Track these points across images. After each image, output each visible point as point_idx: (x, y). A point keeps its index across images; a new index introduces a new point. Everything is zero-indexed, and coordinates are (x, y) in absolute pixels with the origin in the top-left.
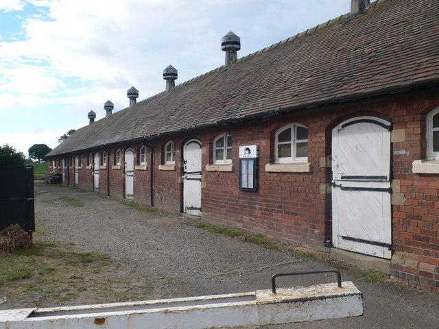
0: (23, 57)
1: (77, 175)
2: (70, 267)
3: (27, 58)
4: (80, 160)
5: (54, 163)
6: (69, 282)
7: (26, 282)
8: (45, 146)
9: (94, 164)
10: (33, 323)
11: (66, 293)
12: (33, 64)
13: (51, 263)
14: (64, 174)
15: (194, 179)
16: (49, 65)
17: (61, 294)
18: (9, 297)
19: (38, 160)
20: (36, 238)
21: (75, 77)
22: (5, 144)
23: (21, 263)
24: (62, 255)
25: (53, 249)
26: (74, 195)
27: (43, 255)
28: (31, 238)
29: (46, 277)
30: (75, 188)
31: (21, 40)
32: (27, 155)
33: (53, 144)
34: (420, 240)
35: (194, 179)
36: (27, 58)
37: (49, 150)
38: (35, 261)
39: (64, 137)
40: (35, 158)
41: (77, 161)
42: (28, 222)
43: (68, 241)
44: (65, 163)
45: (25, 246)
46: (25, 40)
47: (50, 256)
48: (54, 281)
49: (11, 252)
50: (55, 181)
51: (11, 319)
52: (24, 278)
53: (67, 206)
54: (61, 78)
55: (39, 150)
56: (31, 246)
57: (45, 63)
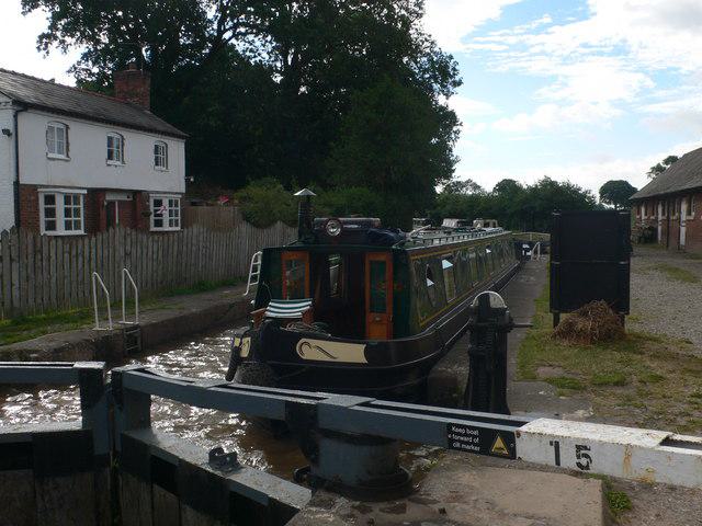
0: (585, 45)
1: (683, 230)
2: (691, 379)
3: (591, 47)
4: (690, 206)
5: (643, 210)
6: (690, 403)
7: (619, 391)
8: (626, 183)
9: (680, 212)
10: (670, 456)
11: (687, 418)
12: (601, 54)
13: (659, 368)
14: (660, 228)
15: (80, 188)
16: (627, 53)
17: (678, 419)
18: (597, 408)
19: (613, 206)
20: (630, 326)
21: (669, 69)
22: (542, 178)
23: (609, 361)
24: (674, 357)
25: (656, 346)
26: (678, 262)
27: (642, 353)
28: (623, 325)
29: (650, 387)
30: (680, 251)
31: (580, 20)
32: (596, 193)
33: (640, 181)
34: (59, 317)
35: (80, 188)
36: (591, 47)
37: (634, 190)
38: (630, 360)
39: (658, 169)
40: (609, 203)
41: (684, 207)
42: (620, 300)
43: (679, 336)
44: (663, 210)
45: (612, 336)
46: (587, 19)
47: (655, 356)
48: (664, 397)
49: (594, 343)
50: (646, 238)
51: (635, 442)
52: (617, 384)
53: (668, 280)
54: (646, 73)
55: (617, 190)
56: (623, 336)
57: (620, 50)
